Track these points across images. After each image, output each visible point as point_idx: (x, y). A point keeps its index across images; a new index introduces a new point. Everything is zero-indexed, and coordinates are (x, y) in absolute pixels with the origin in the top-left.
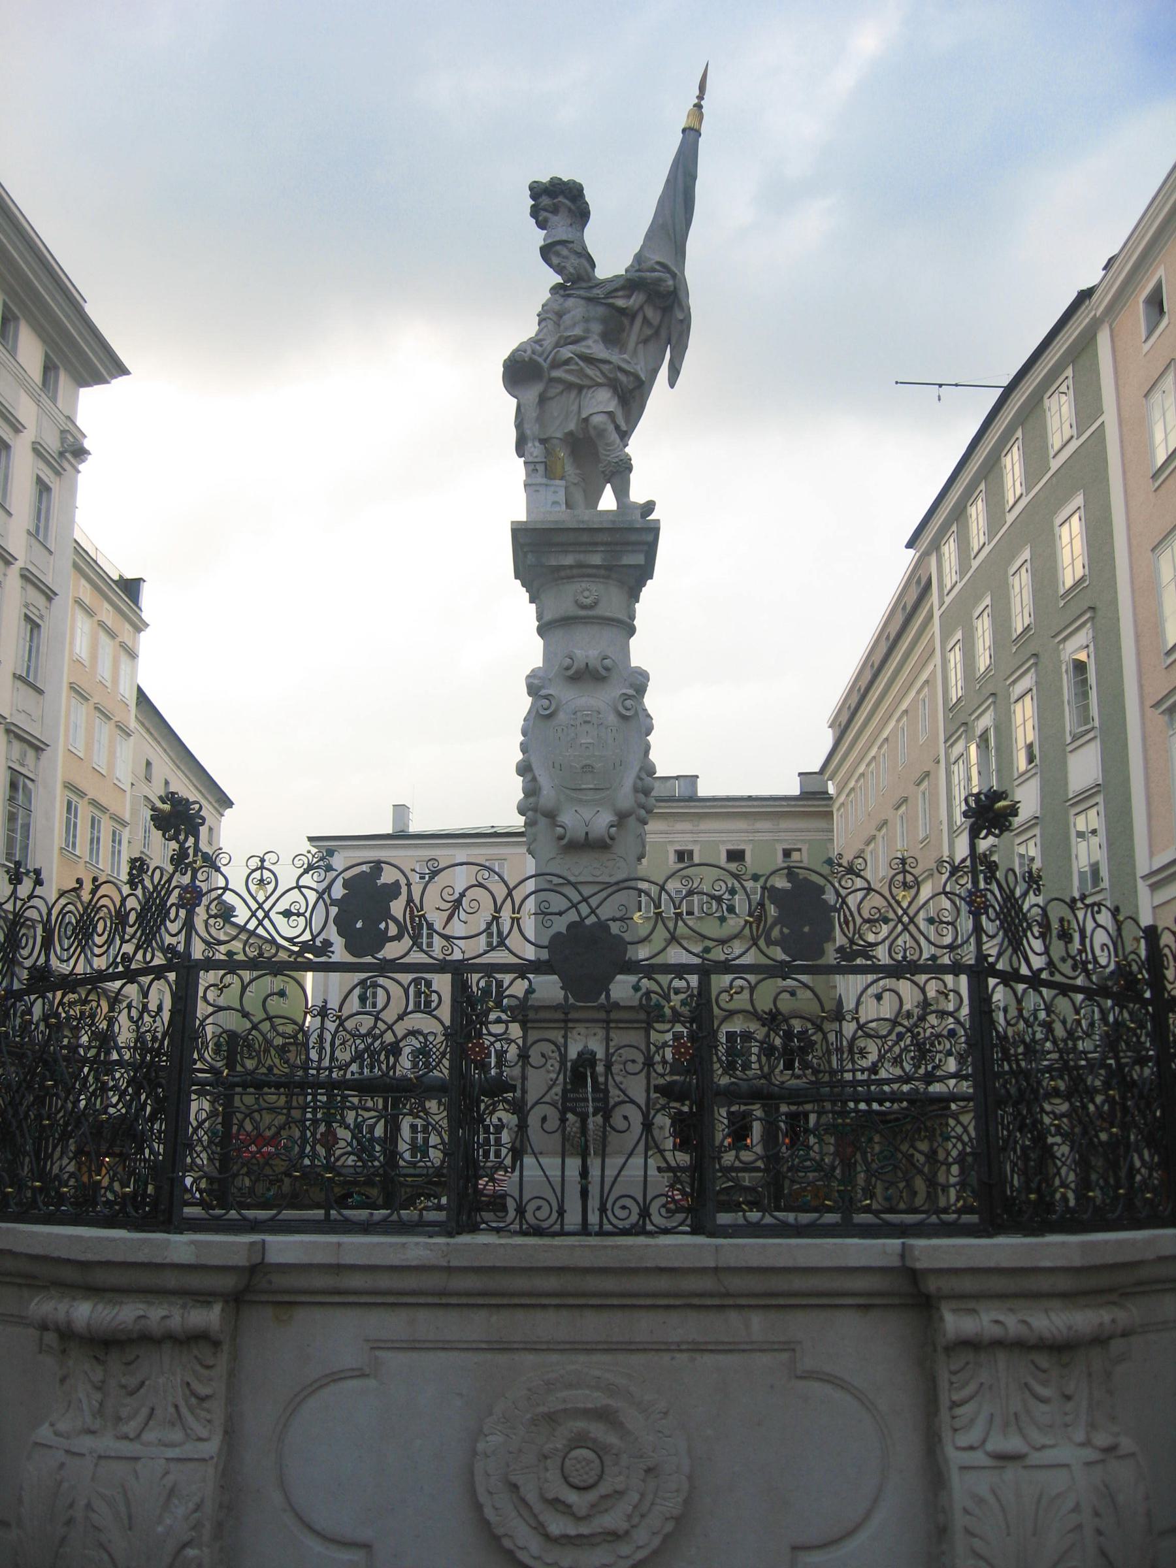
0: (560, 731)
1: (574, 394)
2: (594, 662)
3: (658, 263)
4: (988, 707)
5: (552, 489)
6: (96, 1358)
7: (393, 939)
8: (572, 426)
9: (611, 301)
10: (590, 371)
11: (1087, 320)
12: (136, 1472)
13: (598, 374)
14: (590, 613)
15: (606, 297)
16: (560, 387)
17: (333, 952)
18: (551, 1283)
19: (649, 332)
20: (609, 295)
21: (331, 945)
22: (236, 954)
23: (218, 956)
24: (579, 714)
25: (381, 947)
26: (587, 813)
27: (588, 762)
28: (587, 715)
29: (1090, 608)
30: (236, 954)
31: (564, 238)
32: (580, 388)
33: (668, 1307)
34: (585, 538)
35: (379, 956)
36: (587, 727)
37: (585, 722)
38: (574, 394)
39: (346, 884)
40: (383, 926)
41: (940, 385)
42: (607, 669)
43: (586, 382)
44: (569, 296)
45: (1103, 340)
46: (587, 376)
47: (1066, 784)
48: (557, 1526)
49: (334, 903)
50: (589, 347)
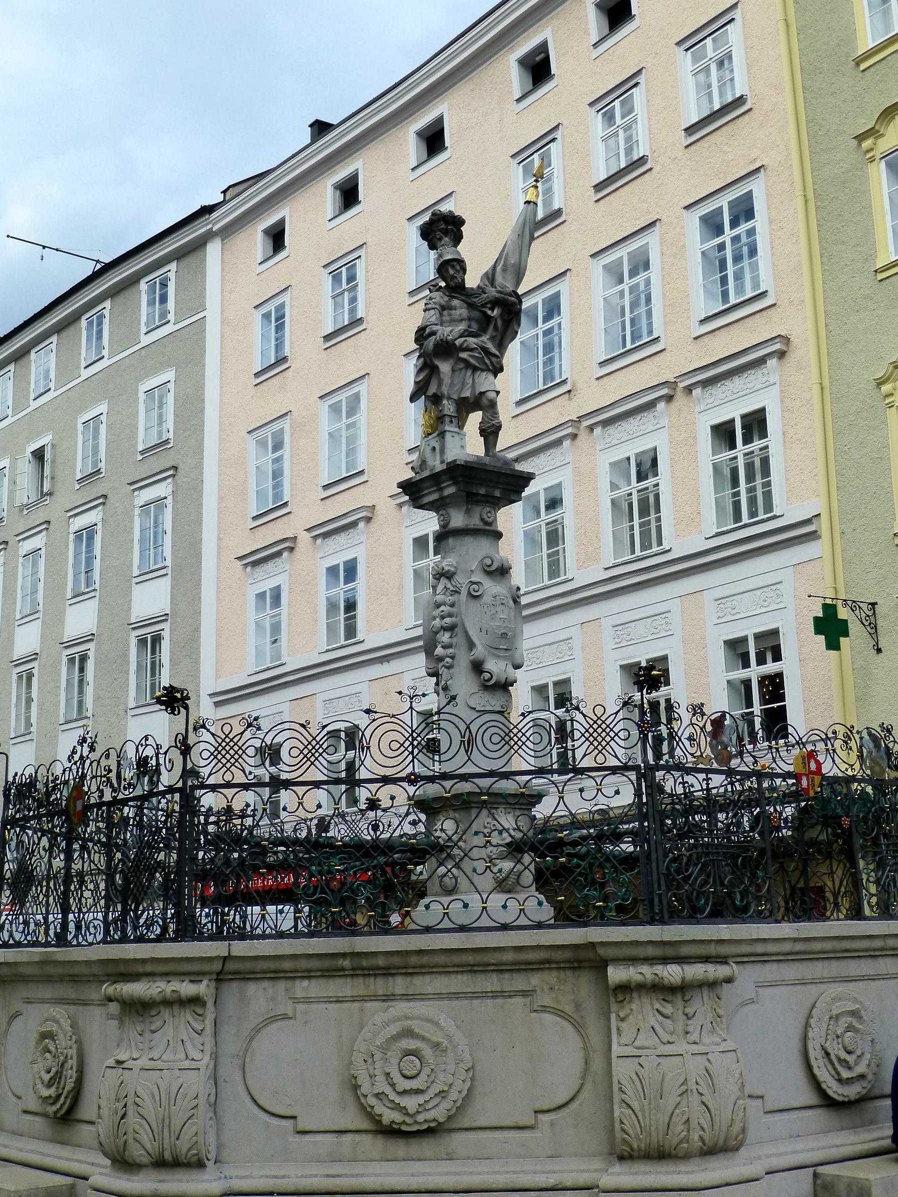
1: (469, 373)
4: (40, 532)
6: (663, 1000)
8: (467, 394)
11: (204, 230)
12: (708, 1060)
14: (488, 528)
18: (828, 946)
20: (484, 306)
32: (475, 369)
33: (859, 957)
36: (502, 607)
41: (44, 247)
43: (482, 366)
45: (213, 249)
48: (845, 1074)
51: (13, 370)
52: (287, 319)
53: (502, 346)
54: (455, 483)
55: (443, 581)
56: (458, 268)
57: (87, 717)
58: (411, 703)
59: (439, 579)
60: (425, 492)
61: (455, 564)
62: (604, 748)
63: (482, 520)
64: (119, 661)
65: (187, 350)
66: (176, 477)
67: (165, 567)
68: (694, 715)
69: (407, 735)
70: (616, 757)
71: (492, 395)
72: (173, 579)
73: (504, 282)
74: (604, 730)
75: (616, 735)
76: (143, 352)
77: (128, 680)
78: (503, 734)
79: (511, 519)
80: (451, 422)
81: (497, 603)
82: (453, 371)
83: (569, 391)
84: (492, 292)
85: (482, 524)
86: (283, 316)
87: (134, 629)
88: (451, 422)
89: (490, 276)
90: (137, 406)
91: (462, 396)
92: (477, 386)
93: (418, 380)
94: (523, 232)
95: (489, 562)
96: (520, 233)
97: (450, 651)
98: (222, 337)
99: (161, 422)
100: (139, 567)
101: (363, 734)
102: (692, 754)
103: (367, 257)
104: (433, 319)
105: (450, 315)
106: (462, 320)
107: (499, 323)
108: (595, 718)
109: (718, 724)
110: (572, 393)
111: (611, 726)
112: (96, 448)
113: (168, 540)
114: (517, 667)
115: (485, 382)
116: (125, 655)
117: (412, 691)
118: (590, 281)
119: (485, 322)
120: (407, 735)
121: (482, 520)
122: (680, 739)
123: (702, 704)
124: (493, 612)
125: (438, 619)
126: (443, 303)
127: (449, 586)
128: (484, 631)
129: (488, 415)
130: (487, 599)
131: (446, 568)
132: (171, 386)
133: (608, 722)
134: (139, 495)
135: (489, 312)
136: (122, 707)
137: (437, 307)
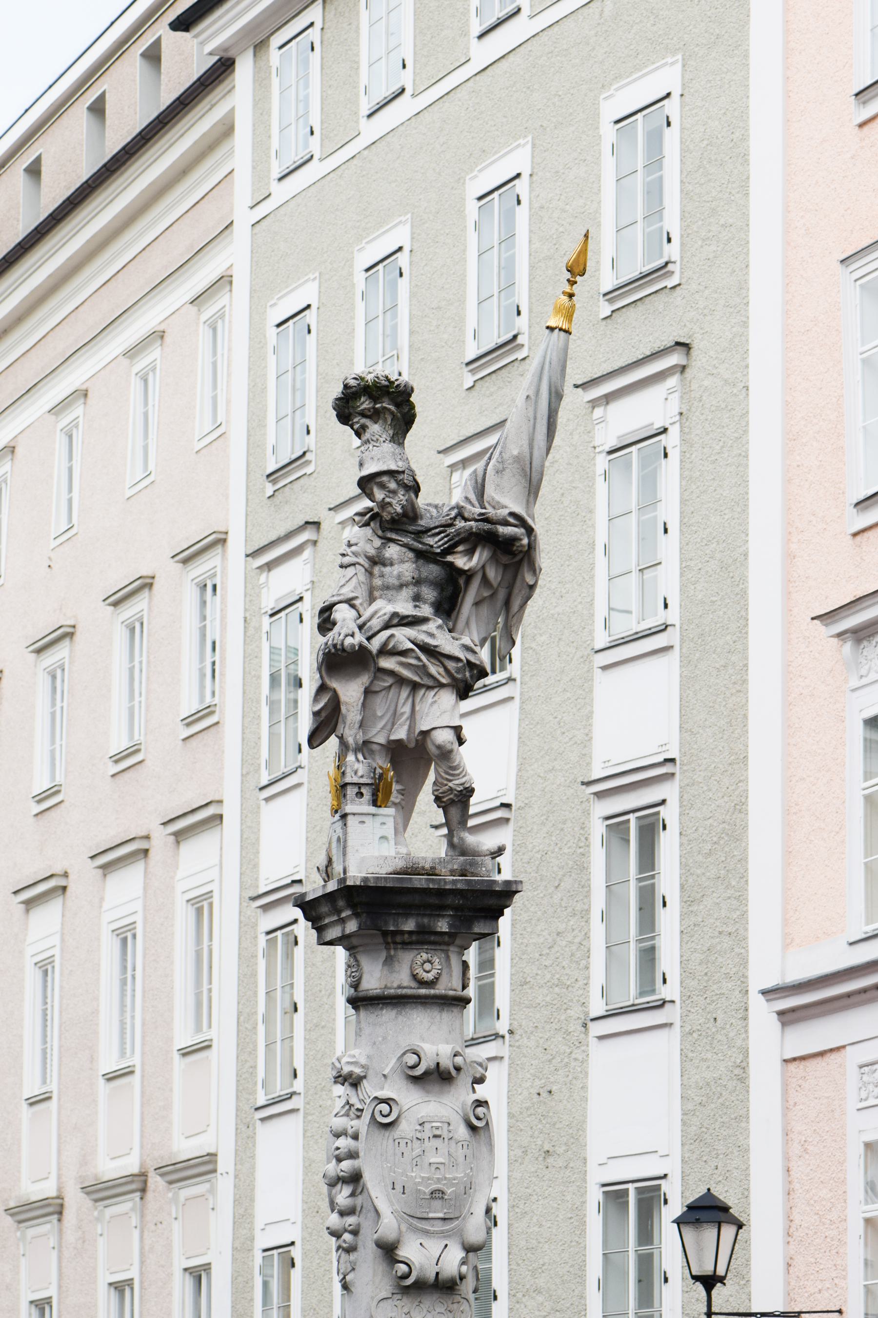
0: (403, 1144)
1: (405, 692)
2: (446, 1063)
3: (512, 514)
5: (379, 819)
8: (401, 734)
10: (433, 669)
13: (441, 670)
16: (389, 681)
19: (486, 594)
24: (427, 1126)
26: (434, 1247)
27: (435, 1187)
28: (437, 1128)
29: (678, 344)
31: (393, 467)
32: (415, 687)
34: (433, 900)
37: (435, 1136)
38: (405, 692)
42: (458, 1069)
43: (430, 683)
46: (431, 676)
50: (432, 635)
51: (318, 25)
54: (356, 915)
56: (393, 485)
57: (497, 1036)
60: (327, 921)
61: (363, 1061)
63: (414, 977)
64: (567, 883)
66: (689, 373)
67: (665, 627)
71: (444, 737)
72: (686, 662)
77: (587, 936)
80: (360, 794)
85: (413, 984)
87: (599, 795)
88: (360, 794)
90: (597, 161)
91: (392, 738)
95: (412, 1059)
96: (531, 393)
97: (351, 1220)
99: (655, 212)
104: (347, 592)
105: (382, 576)
106: (401, 586)
107: (492, 574)
112: (508, 267)
115: (438, 711)
116: (583, 868)
121: (414, 977)
124: (418, 1151)
126: (372, 552)
127: (354, 1100)
128: (399, 1188)
129: (440, 770)
130: (406, 1128)
136: (575, 1012)
137: (361, 560)
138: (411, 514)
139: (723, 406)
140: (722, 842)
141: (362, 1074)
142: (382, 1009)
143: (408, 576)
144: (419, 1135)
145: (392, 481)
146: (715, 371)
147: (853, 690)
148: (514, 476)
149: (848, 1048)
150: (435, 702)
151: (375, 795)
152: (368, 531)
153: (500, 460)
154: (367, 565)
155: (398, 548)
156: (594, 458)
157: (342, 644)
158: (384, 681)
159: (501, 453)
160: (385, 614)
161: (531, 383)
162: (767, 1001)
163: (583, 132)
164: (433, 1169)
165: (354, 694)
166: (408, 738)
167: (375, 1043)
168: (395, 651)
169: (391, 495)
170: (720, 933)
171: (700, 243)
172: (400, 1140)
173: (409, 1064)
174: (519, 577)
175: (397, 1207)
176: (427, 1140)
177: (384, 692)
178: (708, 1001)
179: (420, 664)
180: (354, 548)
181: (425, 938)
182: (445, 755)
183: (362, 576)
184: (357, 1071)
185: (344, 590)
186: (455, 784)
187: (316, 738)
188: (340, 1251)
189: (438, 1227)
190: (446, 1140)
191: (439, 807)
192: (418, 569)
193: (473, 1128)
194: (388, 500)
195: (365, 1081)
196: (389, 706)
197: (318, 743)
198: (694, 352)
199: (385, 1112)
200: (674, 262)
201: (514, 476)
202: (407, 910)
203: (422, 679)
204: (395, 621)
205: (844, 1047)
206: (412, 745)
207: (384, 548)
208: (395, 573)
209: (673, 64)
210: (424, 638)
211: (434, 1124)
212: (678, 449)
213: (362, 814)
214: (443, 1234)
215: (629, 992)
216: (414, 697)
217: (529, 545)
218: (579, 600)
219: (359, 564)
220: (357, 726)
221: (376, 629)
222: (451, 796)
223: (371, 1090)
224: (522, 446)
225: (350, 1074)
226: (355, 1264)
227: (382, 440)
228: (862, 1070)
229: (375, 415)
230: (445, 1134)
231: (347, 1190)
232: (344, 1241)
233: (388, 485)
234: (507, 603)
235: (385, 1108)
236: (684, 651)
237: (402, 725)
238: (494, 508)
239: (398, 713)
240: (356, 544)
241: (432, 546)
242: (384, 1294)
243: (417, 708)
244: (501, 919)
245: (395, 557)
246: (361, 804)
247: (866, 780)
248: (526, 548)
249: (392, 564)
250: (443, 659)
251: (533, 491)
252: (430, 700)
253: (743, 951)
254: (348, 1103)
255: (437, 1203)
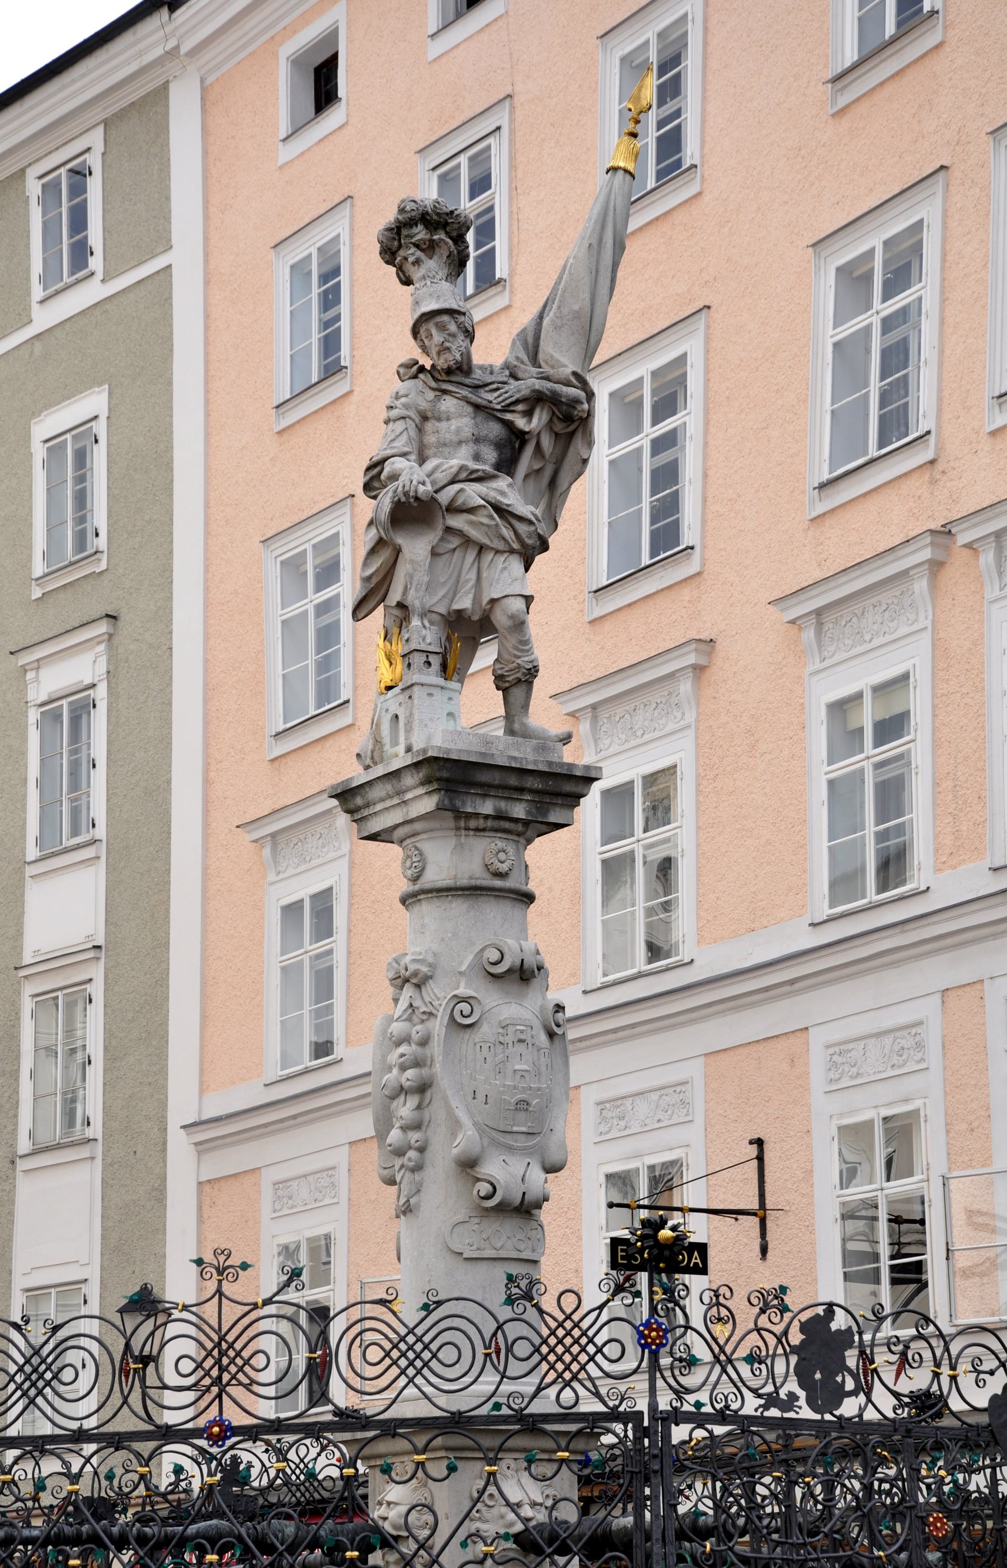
0: (485, 1048)
1: (471, 555)
5: (447, 694)
7: (850, 1394)
8: (464, 602)
9: (508, 416)
15: (505, 410)
17: (800, 1408)
21: (797, 1398)
22: (703, 1405)
23: (686, 1407)
25: (839, 1405)
26: (517, 1166)
27: (520, 1096)
28: (522, 1032)
29: (107, 616)
30: (703, 1405)
31: (455, 306)
35: (837, 1413)
36: (521, 1048)
37: (520, 1041)
39: (804, 1328)
40: (839, 1379)
44: (445, 392)
47: (19, 934)
49: (794, 1350)
50: (503, 493)
52: (344, 278)
53: (553, 491)
55: (408, 991)
56: (453, 327)
58: (220, 1281)
59: (402, 988)
60: (379, 807)
62: (575, 1377)
65: (131, 347)
68: (763, 1311)
69: (209, 1345)
70: (597, 1394)
72: (110, 869)
73: (561, 356)
74: (576, 1341)
75: (600, 1350)
76: (38, 346)
77: (16, 1091)
78: (388, 1346)
79: (565, 859)
81: (508, 1039)
82: (434, 554)
83: (932, 462)
84: (530, 383)
85: (487, 876)
86: (336, 272)
89: (531, 344)
91: (456, 606)
92: (485, 584)
93: (369, 572)
94: (600, 240)
95: (495, 956)
96: (594, 241)
98: (207, 316)
100: (40, 842)
101: (165, 1324)
102: (754, 1391)
103: (512, 132)
104: (400, 445)
106: (460, 442)
107: (547, 442)
108: (561, 1317)
109: (817, 1328)
110: (940, 466)
111: (590, 1333)
113: (99, 780)
114: (552, 1169)
115: (505, 577)
117: (222, 1258)
118: (988, 196)
119: (511, 448)
120: (209, 1345)
122: (730, 1361)
123: (783, 1289)
125: (395, 1071)
126: (424, 405)
128: (481, 1097)
130: (486, 1031)
131: (412, 967)
132: (101, 428)
133: (585, 1325)
134: (37, 679)
135: (521, 423)
137: (412, 414)
138: (465, 367)
139: (148, 665)
140: (144, 1011)
141: (429, 974)
142: (451, 902)
143: (467, 432)
144: (501, 1039)
145: (453, 322)
146: (140, 638)
147: (271, 884)
148: (573, 334)
149: (263, 1170)
150: (505, 568)
151: (444, 666)
152: (417, 383)
153: (558, 314)
154: (417, 421)
155: (455, 401)
156: (26, 712)
157: (416, 491)
158: (449, 542)
159: (559, 307)
160: (451, 467)
161: (593, 230)
162: (188, 1134)
163: (15, 451)
164: (518, 1077)
165: (421, 552)
166: (473, 608)
167: (443, 940)
168: (465, 508)
169: (451, 339)
170: (141, 1083)
171: (126, 536)
172: (482, 1044)
173: (491, 960)
174: (571, 449)
175: (478, 1118)
176: (510, 1045)
177: (447, 555)
178: (129, 1138)
179: (493, 523)
180: (403, 400)
181: (501, 824)
182: (519, 625)
183: (413, 432)
184: (425, 969)
185: (396, 444)
186: (523, 661)
187: (361, 609)
188: (403, 1170)
189: (521, 1142)
190: (530, 1045)
191: (498, 688)
192: (476, 425)
193: (551, 1035)
194: (447, 344)
195: (430, 981)
196: (453, 571)
197: (363, 615)
198: (120, 624)
199: (466, 1012)
200: (102, 552)
201: (573, 334)
202: (486, 790)
203: (492, 541)
204: (463, 475)
205: (260, 1168)
206: (476, 618)
207: (439, 400)
208: (453, 427)
209: (99, 392)
210: (493, 495)
211: (519, 1027)
212: (105, 702)
213: (431, 685)
214: (525, 1151)
215: (57, 1132)
216: (479, 562)
217: (589, 411)
218: (12, 824)
219: (410, 418)
220: (424, 588)
221: (441, 484)
222: (519, 675)
223: (440, 994)
224: (584, 300)
225: (415, 974)
226: (422, 1184)
227: (439, 277)
228: (277, 1187)
229: (429, 248)
230: (529, 1040)
231: (412, 1101)
232: (410, 1159)
233: (449, 327)
234: (553, 483)
235: (465, 1007)
236: (110, 860)
237: (467, 593)
238: (552, 367)
239: (462, 579)
240: (406, 396)
241: (491, 402)
242: (460, 1217)
243: (485, 575)
244: (576, 809)
245: (452, 410)
246: (429, 674)
247: (282, 955)
248: (585, 415)
249: (448, 419)
250: (514, 522)
251: (589, 354)
252: (501, 566)
253: (162, 1097)
254: (411, 1005)
255: (521, 1116)
